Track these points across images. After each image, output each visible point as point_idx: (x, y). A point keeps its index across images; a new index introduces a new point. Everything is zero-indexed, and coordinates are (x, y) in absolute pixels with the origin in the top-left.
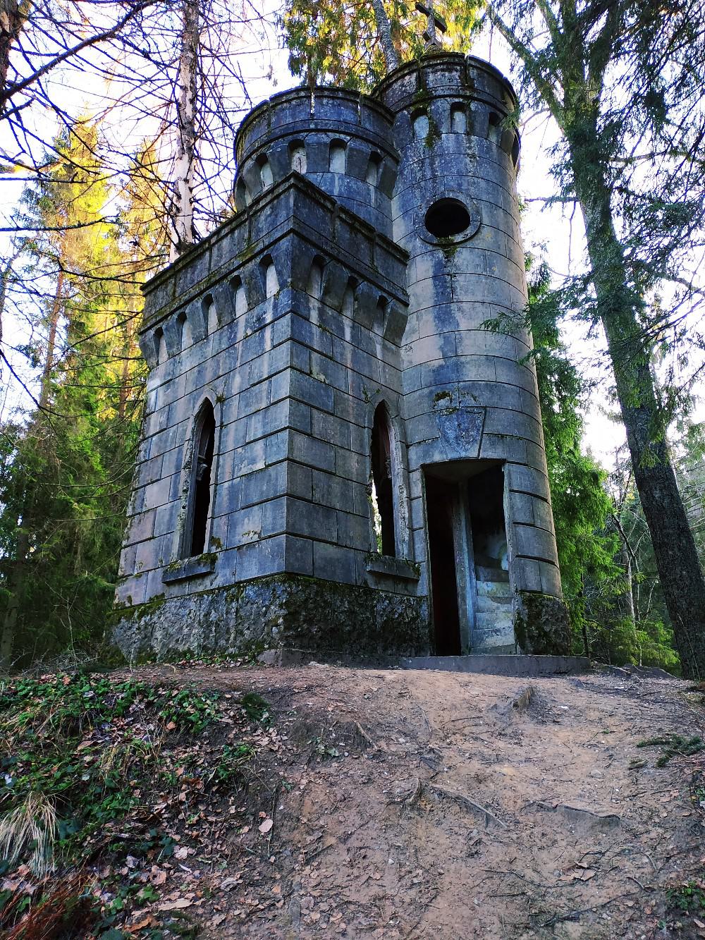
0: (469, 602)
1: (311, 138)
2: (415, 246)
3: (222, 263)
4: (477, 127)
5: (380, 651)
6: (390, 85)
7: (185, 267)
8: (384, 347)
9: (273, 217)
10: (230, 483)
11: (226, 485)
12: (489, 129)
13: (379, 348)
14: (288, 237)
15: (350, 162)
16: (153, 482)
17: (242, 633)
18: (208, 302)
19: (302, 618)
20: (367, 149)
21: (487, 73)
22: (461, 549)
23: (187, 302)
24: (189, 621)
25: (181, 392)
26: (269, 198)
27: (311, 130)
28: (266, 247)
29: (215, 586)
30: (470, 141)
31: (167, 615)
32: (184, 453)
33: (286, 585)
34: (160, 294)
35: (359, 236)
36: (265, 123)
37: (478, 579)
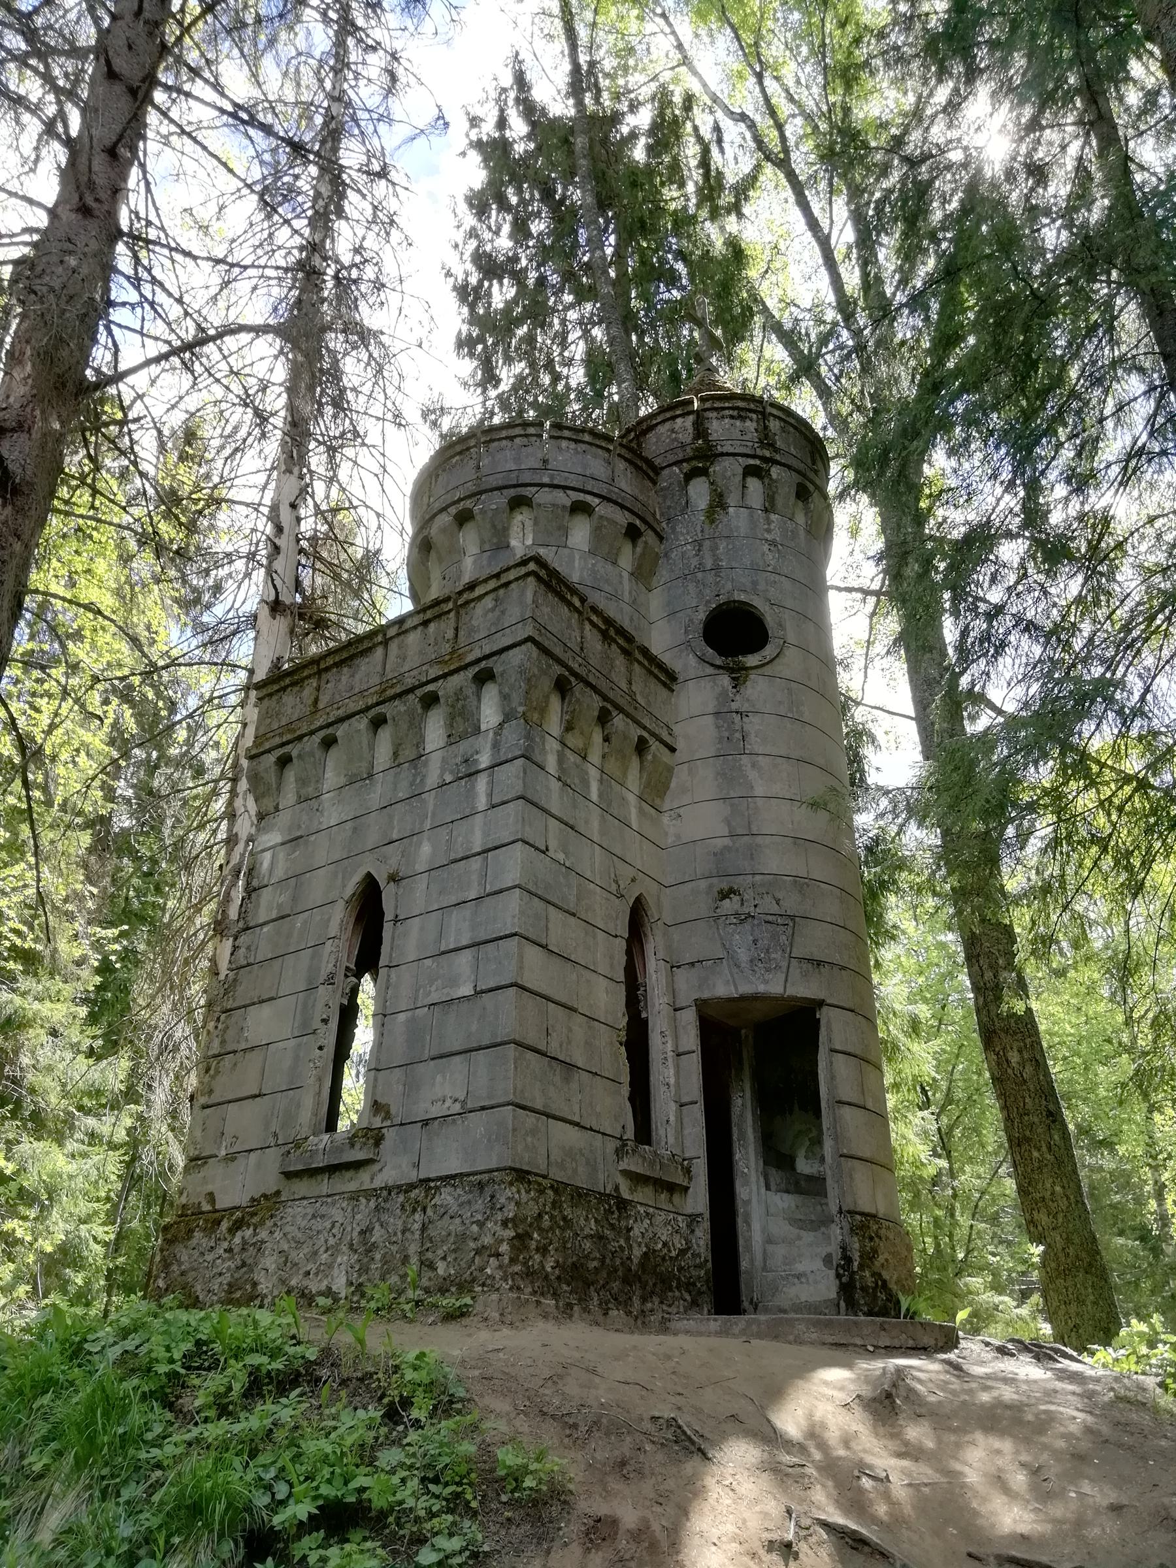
0: (756, 1226)
1: (544, 497)
2: (684, 663)
3: (406, 668)
4: (780, 502)
5: (636, 1301)
6: (651, 428)
7: (338, 665)
8: (641, 811)
9: (497, 613)
10: (409, 1014)
11: (402, 1017)
12: (794, 505)
13: (634, 812)
14: (523, 647)
15: (597, 531)
16: (262, 1002)
17: (431, 1266)
18: (378, 723)
19: (533, 1245)
20: (622, 518)
21: (795, 428)
22: (742, 1136)
23: (341, 720)
24: (332, 1241)
25: (321, 857)
26: (492, 584)
27: (542, 485)
28: (487, 657)
29: (378, 1183)
30: (769, 522)
31: (288, 1229)
32: (325, 958)
33: (514, 1189)
34: (289, 699)
35: (614, 647)
36: (472, 463)
37: (768, 1188)
